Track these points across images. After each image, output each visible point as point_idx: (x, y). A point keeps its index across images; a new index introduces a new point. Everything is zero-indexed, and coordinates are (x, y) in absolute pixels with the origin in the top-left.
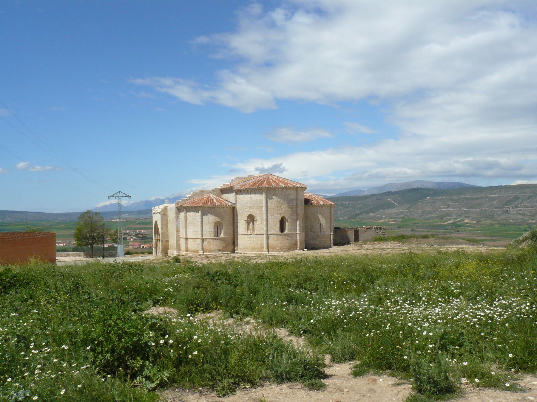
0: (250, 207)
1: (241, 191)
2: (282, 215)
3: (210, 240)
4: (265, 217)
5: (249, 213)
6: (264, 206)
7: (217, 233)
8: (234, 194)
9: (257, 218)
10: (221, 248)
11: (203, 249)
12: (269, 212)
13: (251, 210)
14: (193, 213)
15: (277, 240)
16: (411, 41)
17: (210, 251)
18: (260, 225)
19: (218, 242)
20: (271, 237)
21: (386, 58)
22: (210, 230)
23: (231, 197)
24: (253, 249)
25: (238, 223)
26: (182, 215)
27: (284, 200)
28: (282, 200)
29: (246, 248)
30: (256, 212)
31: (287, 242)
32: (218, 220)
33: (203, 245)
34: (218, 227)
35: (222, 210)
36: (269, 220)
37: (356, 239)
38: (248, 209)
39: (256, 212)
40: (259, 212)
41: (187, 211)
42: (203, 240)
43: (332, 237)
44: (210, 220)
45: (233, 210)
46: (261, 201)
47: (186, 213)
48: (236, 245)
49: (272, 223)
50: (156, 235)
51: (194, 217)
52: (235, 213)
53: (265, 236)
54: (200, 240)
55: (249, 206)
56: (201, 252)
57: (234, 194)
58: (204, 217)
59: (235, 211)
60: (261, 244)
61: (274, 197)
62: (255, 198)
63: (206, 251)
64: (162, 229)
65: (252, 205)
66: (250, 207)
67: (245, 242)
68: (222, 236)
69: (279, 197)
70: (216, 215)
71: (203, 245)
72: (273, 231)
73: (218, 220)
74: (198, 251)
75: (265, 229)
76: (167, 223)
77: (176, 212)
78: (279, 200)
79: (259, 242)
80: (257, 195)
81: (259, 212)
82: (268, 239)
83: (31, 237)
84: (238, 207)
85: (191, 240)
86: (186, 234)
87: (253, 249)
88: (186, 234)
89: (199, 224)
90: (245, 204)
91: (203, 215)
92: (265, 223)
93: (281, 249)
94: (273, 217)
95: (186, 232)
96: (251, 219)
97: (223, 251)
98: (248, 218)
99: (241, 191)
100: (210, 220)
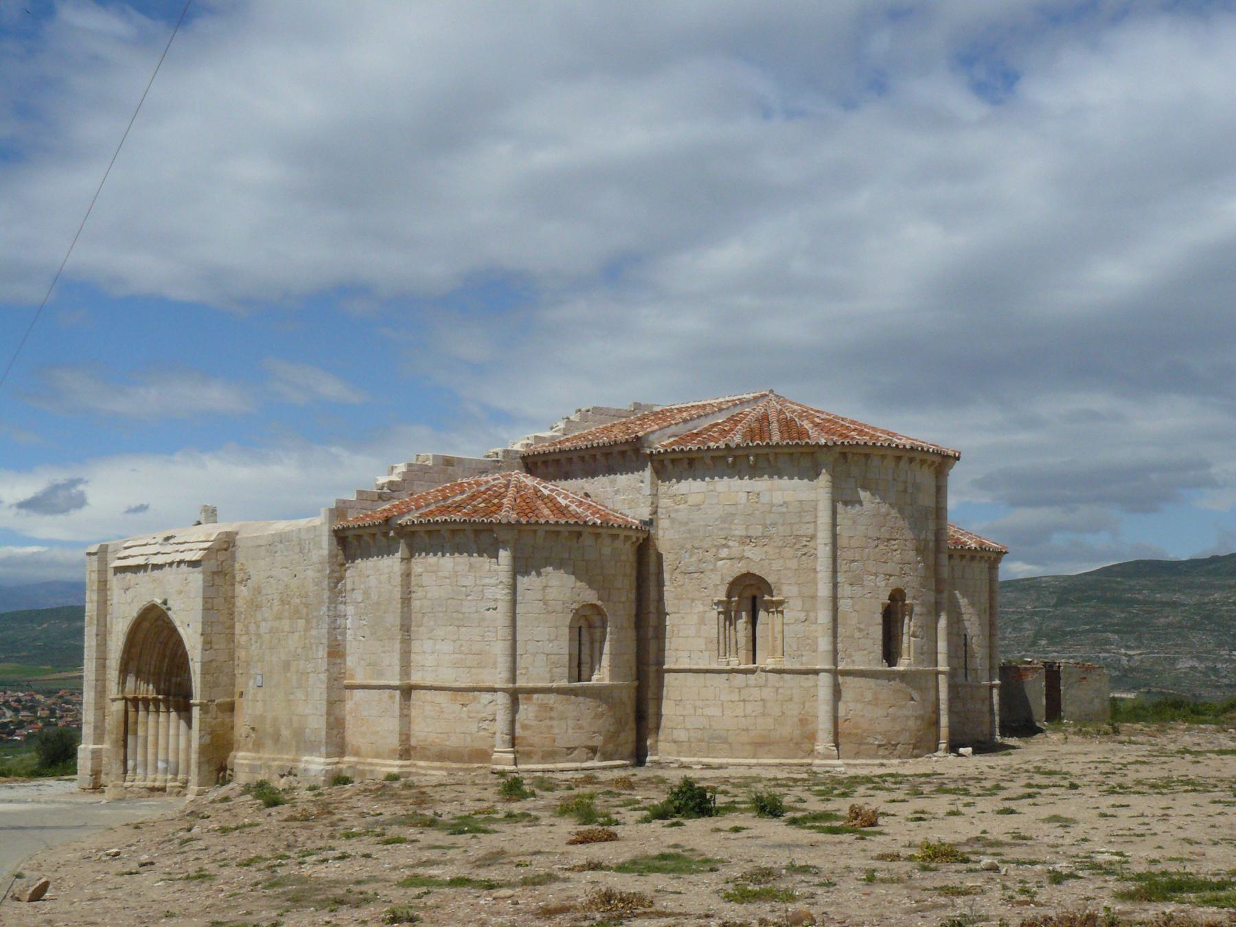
0: (747, 540)
1: (691, 462)
2: (895, 582)
3: (551, 699)
4: (824, 590)
5: (740, 568)
6: (823, 536)
7: (580, 666)
8: (648, 473)
9: (786, 590)
10: (598, 741)
11: (513, 742)
12: (842, 566)
13: (749, 551)
14: (462, 560)
15: (875, 702)
16: (454, 119)
17: (550, 756)
18: (797, 630)
19: (586, 707)
20: (850, 686)
21: (352, 168)
22: (549, 648)
23: (623, 496)
24: (761, 745)
25: (662, 614)
26: (378, 573)
27: (901, 511)
28: (894, 513)
29: (714, 740)
30: (777, 565)
31: (908, 714)
32: (591, 596)
33: (513, 722)
34: (586, 629)
35: (607, 551)
36: (841, 603)
37: (1054, 712)
38: (735, 548)
39: (777, 565)
40: (793, 564)
41: (413, 551)
42: (515, 696)
43: (996, 699)
44: (552, 594)
45: (643, 551)
46: (806, 510)
47: (407, 560)
48: (651, 723)
49: (853, 620)
50: (131, 680)
51: (469, 583)
52: (652, 568)
53: (825, 680)
54: (502, 699)
55: (740, 531)
56: (503, 760)
57: (648, 473)
58: (523, 582)
59: (653, 559)
60: (803, 722)
61: (864, 495)
62: (778, 497)
63: (528, 756)
64: (208, 644)
65: (756, 531)
66: (747, 540)
67: (715, 711)
68: (602, 676)
69: (884, 499)
70: (584, 571)
71: (513, 722)
72: (857, 656)
73: (591, 596)
74: (483, 755)
75: (824, 644)
76: (231, 615)
77: (332, 556)
78: (884, 508)
79: (793, 710)
80: (785, 482)
81: (793, 564)
82: (837, 693)
83: (3, 615)
84: (666, 538)
85: (441, 697)
86: (406, 666)
87: (761, 745)
88: (406, 666)
89: (500, 617)
90: (706, 526)
91: (521, 567)
92: (824, 616)
93: (889, 747)
94: (858, 590)
95: (406, 655)
96: (749, 597)
97: (606, 757)
98: (729, 595)
99: (691, 462)
100: (552, 594)
